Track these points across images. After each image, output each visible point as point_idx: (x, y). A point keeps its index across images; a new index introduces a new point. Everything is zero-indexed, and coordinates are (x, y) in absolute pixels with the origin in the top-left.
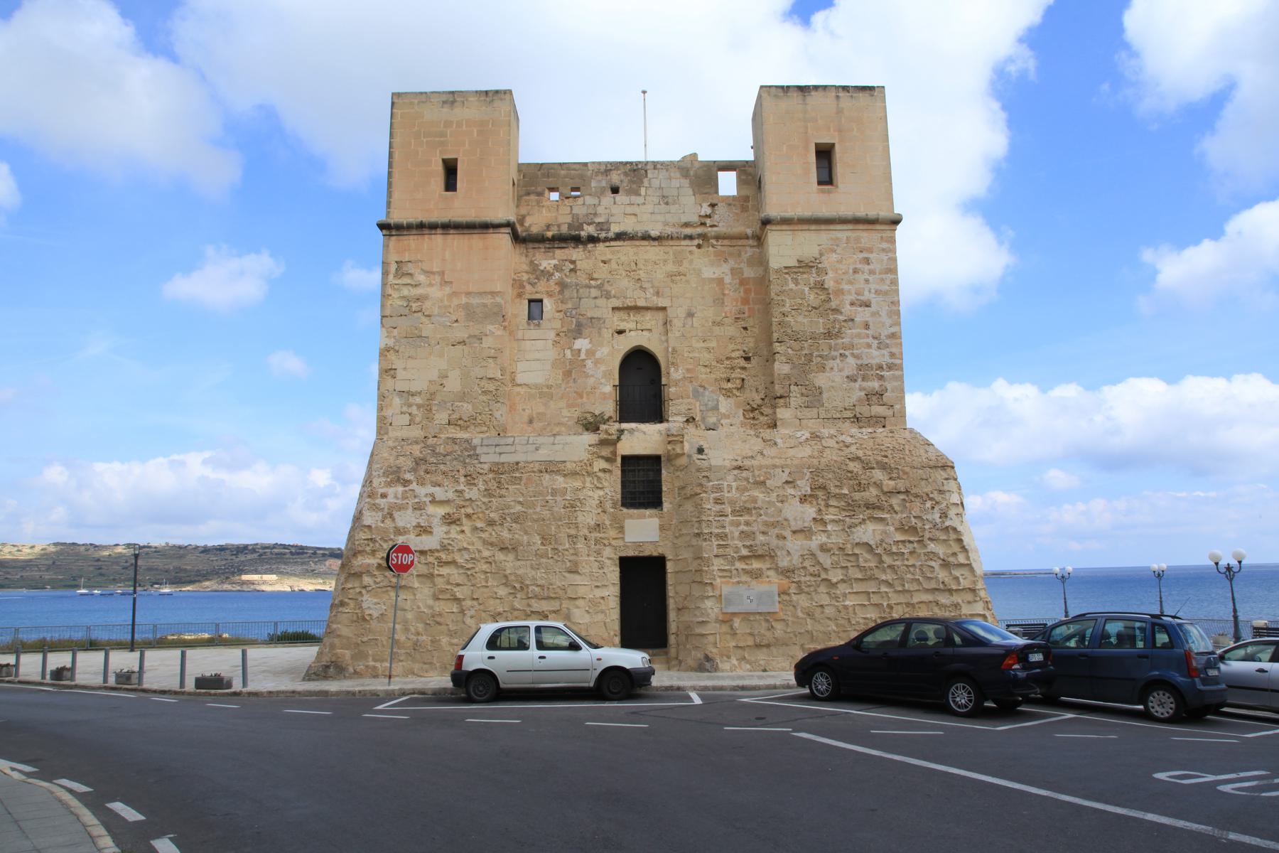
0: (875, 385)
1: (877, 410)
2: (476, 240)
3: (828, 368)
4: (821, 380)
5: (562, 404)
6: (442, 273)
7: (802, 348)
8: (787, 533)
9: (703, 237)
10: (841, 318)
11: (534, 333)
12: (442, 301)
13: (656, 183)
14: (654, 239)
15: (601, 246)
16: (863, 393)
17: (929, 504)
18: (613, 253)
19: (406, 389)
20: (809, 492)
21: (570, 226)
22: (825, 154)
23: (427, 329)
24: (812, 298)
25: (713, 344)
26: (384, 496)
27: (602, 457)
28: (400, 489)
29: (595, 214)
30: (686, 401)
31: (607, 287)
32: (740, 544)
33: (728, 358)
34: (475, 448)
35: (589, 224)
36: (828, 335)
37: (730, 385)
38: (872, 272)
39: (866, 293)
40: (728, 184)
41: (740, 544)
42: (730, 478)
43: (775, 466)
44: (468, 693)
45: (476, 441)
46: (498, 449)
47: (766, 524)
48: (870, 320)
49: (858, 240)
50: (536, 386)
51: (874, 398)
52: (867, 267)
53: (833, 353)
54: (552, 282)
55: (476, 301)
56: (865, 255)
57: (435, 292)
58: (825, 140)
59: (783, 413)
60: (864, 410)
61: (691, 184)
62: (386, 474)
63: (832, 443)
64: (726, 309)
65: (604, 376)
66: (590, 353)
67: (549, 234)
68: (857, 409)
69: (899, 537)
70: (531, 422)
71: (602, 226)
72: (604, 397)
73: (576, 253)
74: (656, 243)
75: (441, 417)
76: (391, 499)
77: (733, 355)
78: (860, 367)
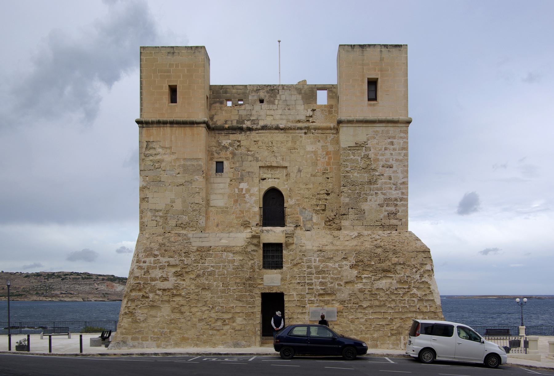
0: (392, 209)
2: (188, 130)
4: (365, 206)
5: (233, 216)
7: (356, 190)
8: (342, 283)
9: (308, 128)
10: (377, 174)
11: (219, 180)
14: (282, 129)
15: (254, 133)
16: (386, 213)
17: (414, 270)
22: (373, 83)
23: (164, 177)
25: (311, 186)
26: (145, 262)
27: (253, 244)
28: (152, 259)
29: (251, 115)
31: (257, 155)
32: (319, 288)
34: (189, 239)
35: (248, 120)
36: (370, 183)
38: (394, 149)
39: (391, 160)
40: (322, 98)
41: (319, 288)
42: (315, 255)
43: (337, 250)
45: (190, 235)
46: (201, 239)
47: (332, 278)
48: (392, 175)
49: (388, 132)
50: (220, 208)
51: (392, 216)
54: (228, 153)
55: (189, 163)
57: (168, 158)
59: (345, 223)
60: (387, 222)
61: (303, 98)
63: (368, 238)
64: (318, 168)
66: (248, 190)
68: (383, 221)
70: (218, 225)
72: (255, 213)
74: (283, 131)
75: (173, 223)
78: (385, 200)
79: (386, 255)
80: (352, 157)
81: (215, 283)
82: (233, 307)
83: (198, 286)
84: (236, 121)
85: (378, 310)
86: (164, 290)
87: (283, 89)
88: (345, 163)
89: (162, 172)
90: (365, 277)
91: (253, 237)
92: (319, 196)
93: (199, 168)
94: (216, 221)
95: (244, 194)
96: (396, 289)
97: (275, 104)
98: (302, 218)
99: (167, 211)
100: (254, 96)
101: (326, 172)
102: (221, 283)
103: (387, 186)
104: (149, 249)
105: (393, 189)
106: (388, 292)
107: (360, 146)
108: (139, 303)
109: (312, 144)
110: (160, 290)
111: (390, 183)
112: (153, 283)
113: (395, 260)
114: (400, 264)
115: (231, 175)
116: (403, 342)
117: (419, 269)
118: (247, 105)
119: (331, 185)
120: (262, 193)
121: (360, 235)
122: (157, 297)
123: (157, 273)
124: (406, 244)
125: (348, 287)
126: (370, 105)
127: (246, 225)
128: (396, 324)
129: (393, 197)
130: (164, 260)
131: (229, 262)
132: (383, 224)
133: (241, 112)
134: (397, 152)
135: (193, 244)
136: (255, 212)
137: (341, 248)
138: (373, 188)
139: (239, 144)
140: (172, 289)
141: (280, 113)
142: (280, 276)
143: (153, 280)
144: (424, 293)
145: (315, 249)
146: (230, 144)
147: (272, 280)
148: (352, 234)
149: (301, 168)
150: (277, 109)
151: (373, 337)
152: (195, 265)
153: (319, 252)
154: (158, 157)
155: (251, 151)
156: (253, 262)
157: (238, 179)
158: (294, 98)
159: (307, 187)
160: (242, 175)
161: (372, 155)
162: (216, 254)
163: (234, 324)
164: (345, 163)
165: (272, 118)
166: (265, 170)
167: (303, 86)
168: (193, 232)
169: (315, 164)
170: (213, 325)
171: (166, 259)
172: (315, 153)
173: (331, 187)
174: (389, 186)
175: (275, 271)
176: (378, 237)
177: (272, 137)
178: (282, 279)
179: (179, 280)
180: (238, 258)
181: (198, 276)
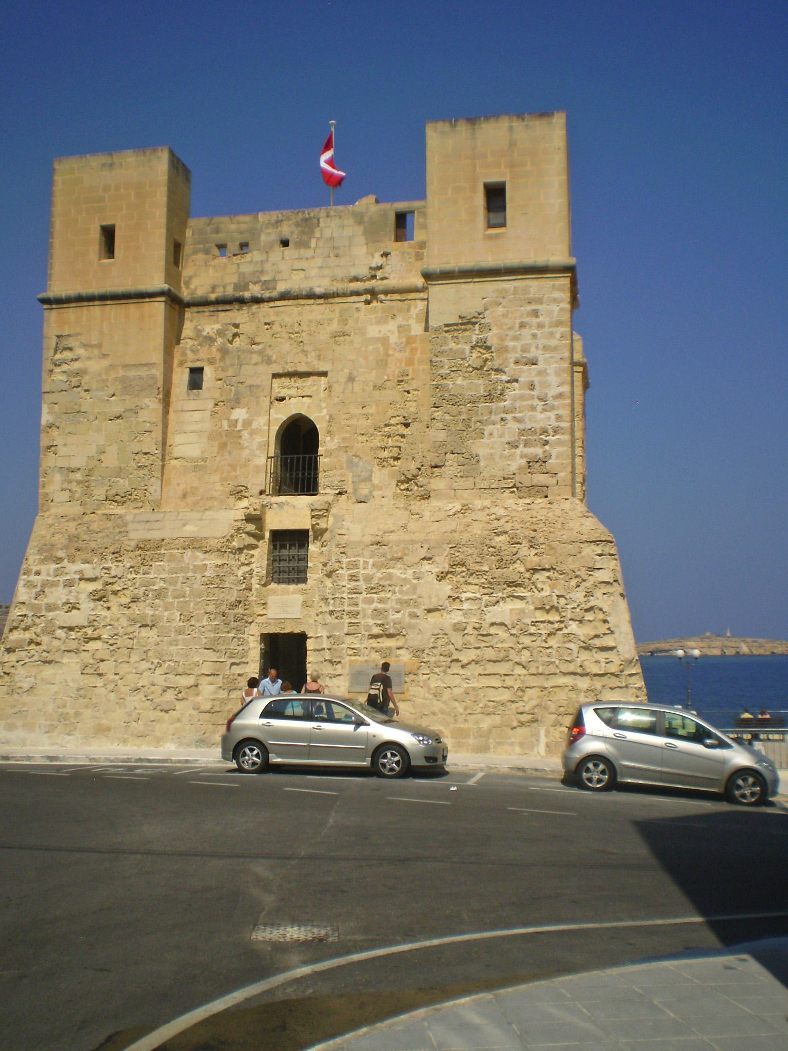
0: (538, 451)
1: (540, 479)
2: (133, 308)
3: (486, 433)
4: (481, 448)
5: (216, 477)
6: (99, 346)
7: (460, 413)
8: (419, 612)
9: (373, 293)
10: (505, 378)
11: (192, 405)
12: (100, 375)
13: (327, 233)
14: (320, 297)
15: (265, 307)
16: (523, 462)
17: (573, 583)
18: (277, 314)
19: (66, 466)
20: (447, 568)
21: (237, 287)
23: (87, 402)
24: (474, 358)
25: (371, 410)
26: (38, 573)
28: (53, 566)
29: (262, 272)
30: (339, 472)
31: (269, 352)
32: (371, 622)
33: (386, 425)
34: (125, 525)
35: (255, 283)
37: (386, 454)
38: (540, 326)
39: (533, 349)
41: (371, 622)
42: (367, 552)
43: (413, 542)
44: (238, 763)
45: (129, 518)
46: (147, 526)
47: (400, 601)
48: (536, 380)
49: (526, 290)
50: (192, 460)
52: (535, 321)
53: (493, 417)
54: (214, 349)
55: (132, 373)
56: (534, 307)
57: (95, 366)
58: (494, 179)
59: (438, 484)
60: (527, 480)
61: (365, 232)
62: (40, 552)
63: (481, 516)
64: (389, 371)
65: (260, 447)
66: (247, 423)
67: (213, 297)
68: (517, 478)
69: (540, 616)
70: (184, 496)
71: (266, 285)
72: (257, 469)
73: (240, 315)
74: (322, 301)
75: (100, 492)
76: (43, 577)
77: (393, 421)
78: (522, 432)
79: (515, 550)
80: (452, 345)
81: (166, 614)
82: (197, 664)
83: (133, 621)
84: (232, 286)
85: (491, 668)
86: (71, 629)
87: (328, 216)
88: (438, 359)
89: (84, 394)
90: (468, 599)
91: (249, 519)
92: (387, 429)
93: (151, 382)
94: (182, 486)
95: (240, 431)
96: (534, 623)
97: (309, 247)
98: (351, 475)
99: (90, 470)
100: (269, 234)
101: (405, 378)
102: (178, 614)
103: (525, 403)
104: (49, 546)
105: (539, 408)
106: (513, 631)
107: (469, 323)
108: (23, 654)
109: (378, 323)
110: (62, 628)
111: (532, 397)
112: (51, 615)
113: (534, 561)
114: (543, 570)
115: (217, 395)
116: (543, 740)
117: (584, 581)
118: (256, 252)
119: (414, 404)
120: (275, 428)
121: (465, 509)
122: (56, 643)
123: (59, 595)
124: (559, 525)
125: (432, 618)
126: (490, 237)
127: (239, 493)
128: (532, 698)
129: (538, 426)
130: (73, 568)
131: (196, 569)
132: (518, 485)
133: (243, 269)
134: (547, 330)
135: (132, 535)
136: (258, 466)
137: (419, 536)
138: (497, 408)
139: (235, 330)
140: (84, 627)
141: (319, 264)
142: (300, 598)
143: (51, 608)
144: (592, 633)
145: (368, 539)
146: (220, 333)
147: (285, 608)
148: (450, 506)
149: (355, 374)
150: (313, 257)
151: (480, 729)
152: (131, 576)
153: (375, 546)
154: (76, 365)
155: (258, 344)
156: (246, 569)
157: (230, 400)
158: (348, 232)
159: (365, 411)
160: (237, 393)
161: (492, 337)
162: (171, 555)
163: (200, 698)
164: (438, 359)
165: (302, 274)
166: (285, 381)
167: (367, 209)
168: (137, 511)
169: (382, 363)
170: (157, 701)
171: (79, 566)
172: (384, 340)
173: (412, 409)
174: (529, 403)
175: (292, 587)
176: (501, 512)
177: (300, 314)
178: (306, 605)
179: (100, 607)
180: (212, 561)
181: (135, 600)
